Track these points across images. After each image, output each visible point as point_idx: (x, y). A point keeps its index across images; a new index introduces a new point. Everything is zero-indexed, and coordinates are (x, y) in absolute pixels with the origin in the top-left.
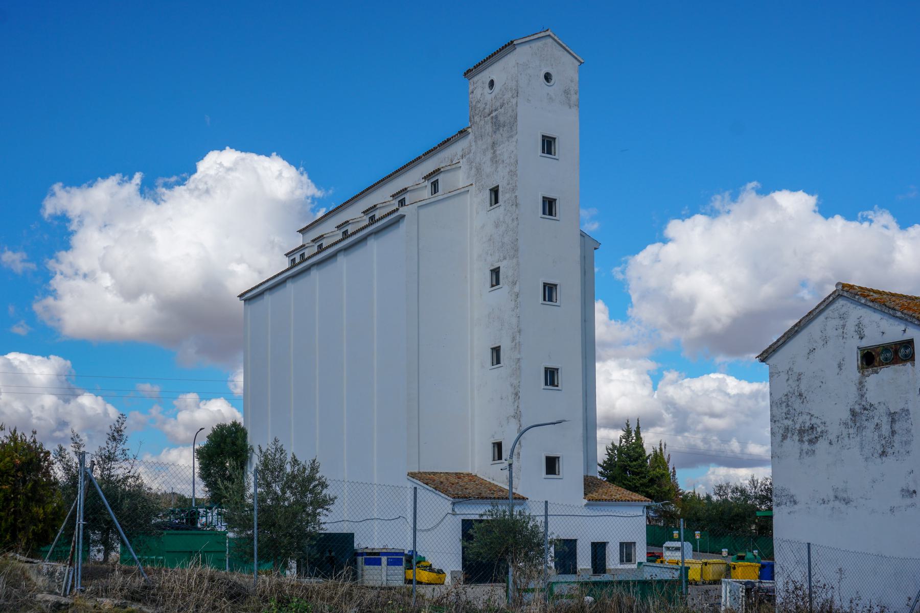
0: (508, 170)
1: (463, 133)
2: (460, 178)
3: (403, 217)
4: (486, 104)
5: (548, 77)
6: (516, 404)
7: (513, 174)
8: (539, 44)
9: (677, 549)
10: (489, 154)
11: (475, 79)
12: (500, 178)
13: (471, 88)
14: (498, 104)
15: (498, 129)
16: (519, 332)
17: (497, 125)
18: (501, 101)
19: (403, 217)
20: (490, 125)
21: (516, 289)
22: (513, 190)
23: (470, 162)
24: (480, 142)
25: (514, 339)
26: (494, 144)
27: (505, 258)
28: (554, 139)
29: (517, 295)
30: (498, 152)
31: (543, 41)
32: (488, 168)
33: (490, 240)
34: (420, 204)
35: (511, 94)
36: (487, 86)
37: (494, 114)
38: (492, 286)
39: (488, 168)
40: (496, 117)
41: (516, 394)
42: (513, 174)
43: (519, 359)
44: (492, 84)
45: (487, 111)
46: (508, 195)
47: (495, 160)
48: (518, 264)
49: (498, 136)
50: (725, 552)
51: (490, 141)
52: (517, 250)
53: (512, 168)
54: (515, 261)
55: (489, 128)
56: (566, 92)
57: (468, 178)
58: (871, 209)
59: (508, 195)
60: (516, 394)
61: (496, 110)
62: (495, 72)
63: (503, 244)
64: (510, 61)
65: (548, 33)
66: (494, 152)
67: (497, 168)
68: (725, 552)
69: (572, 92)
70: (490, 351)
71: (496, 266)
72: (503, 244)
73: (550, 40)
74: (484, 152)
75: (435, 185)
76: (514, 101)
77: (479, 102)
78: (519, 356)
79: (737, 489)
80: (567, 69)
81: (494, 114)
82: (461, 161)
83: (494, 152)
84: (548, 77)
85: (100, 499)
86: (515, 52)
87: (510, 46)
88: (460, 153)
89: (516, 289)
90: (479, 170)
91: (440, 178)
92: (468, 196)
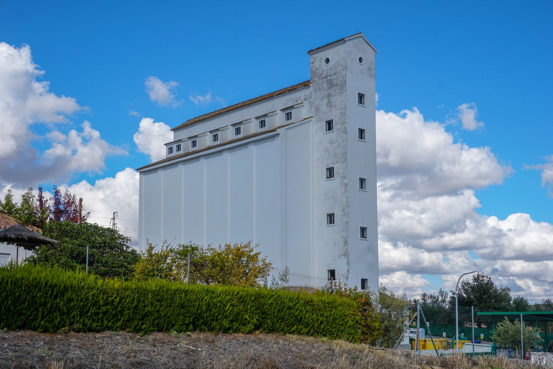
0: (339, 111)
1: (306, 85)
2: (303, 112)
3: (278, 134)
4: (323, 71)
5: (360, 60)
6: (345, 248)
7: (343, 114)
8: (356, 40)
9: (415, 332)
10: (325, 101)
11: (315, 56)
12: (334, 115)
13: (312, 60)
14: (332, 73)
15: (332, 87)
16: (348, 206)
17: (331, 85)
18: (335, 71)
19: (278, 134)
20: (326, 84)
21: (346, 181)
22: (344, 123)
23: (311, 104)
24: (318, 93)
25: (344, 210)
26: (329, 95)
27: (337, 162)
28: (364, 95)
29: (346, 185)
30: (332, 100)
31: (358, 39)
32: (324, 108)
33: (326, 150)
34: (287, 127)
35: (341, 69)
36: (324, 61)
37: (329, 78)
38: (328, 178)
39: (324, 108)
40: (331, 80)
41: (346, 242)
42: (343, 114)
43: (347, 222)
44: (327, 61)
45: (324, 75)
46: (339, 126)
47: (329, 104)
48: (347, 166)
49: (332, 91)
50: (444, 334)
51: (326, 93)
52: (346, 159)
53: (343, 111)
54: (345, 164)
55: (325, 85)
56: (369, 69)
57: (309, 112)
58: (410, 109)
59: (339, 126)
60: (346, 242)
61: (330, 76)
62: (329, 53)
63: (336, 154)
64: (341, 49)
65: (361, 35)
66: (329, 100)
67: (331, 109)
68: (444, 334)
69: (372, 69)
70: (326, 216)
71: (331, 166)
72: (336, 154)
73: (361, 39)
74: (322, 99)
75: (289, 116)
76: (344, 73)
77: (318, 69)
78: (347, 220)
79: (431, 296)
80: (369, 56)
81: (329, 78)
82: (304, 102)
83: (329, 100)
84: (360, 60)
85: (471, 313)
86: (344, 45)
87: (342, 41)
88: (303, 97)
89: (346, 181)
90: (317, 109)
91: (293, 111)
92: (311, 123)
